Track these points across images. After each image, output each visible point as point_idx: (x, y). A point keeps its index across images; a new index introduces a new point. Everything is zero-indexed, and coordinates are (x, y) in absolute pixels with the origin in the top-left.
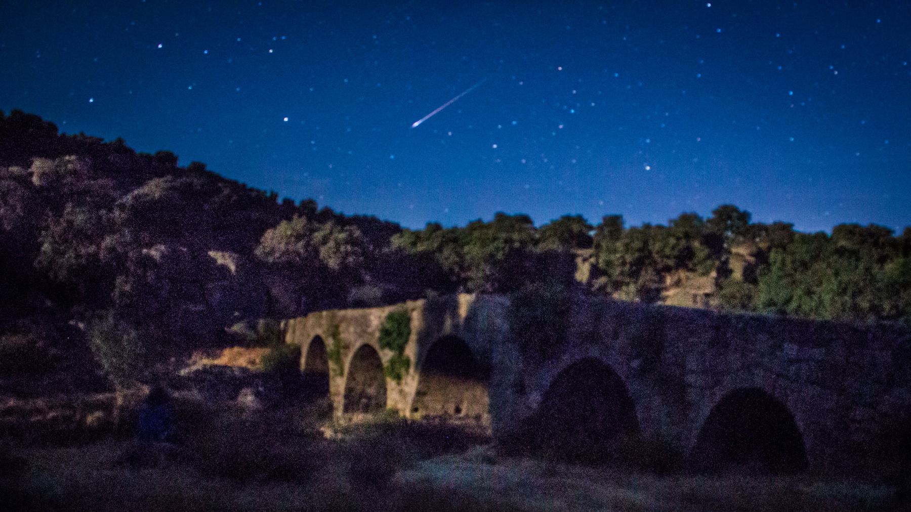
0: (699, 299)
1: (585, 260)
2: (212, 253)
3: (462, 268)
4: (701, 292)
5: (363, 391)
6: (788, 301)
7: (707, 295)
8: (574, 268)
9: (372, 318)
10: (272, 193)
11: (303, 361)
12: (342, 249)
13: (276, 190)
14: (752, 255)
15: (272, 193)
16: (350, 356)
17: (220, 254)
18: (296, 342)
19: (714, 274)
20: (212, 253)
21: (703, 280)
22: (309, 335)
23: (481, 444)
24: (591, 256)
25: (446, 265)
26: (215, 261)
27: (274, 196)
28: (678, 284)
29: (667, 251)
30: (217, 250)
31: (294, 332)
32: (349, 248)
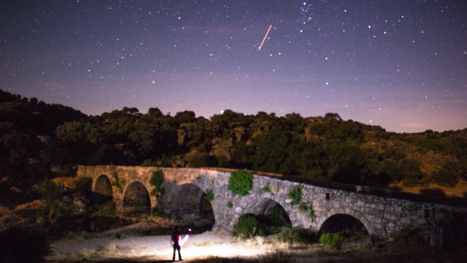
0: (227, 149)
1: (182, 134)
2: (39, 137)
3: (140, 141)
4: (228, 146)
5: (130, 198)
6: (269, 153)
7: (230, 147)
8: (177, 137)
9: (139, 171)
10: (18, 95)
11: (94, 184)
12: (97, 134)
13: (20, 94)
14: (244, 131)
15: (18, 95)
16: (127, 186)
17: (43, 137)
18: (87, 175)
19: (231, 139)
20: (39, 137)
21: (228, 142)
22: (97, 174)
23: (59, 177)
24: (184, 133)
25: (134, 139)
26: (40, 140)
27: (15, 95)
28: (217, 143)
29: (213, 130)
30: (41, 135)
31: (300, 248)
32: (99, 134)
